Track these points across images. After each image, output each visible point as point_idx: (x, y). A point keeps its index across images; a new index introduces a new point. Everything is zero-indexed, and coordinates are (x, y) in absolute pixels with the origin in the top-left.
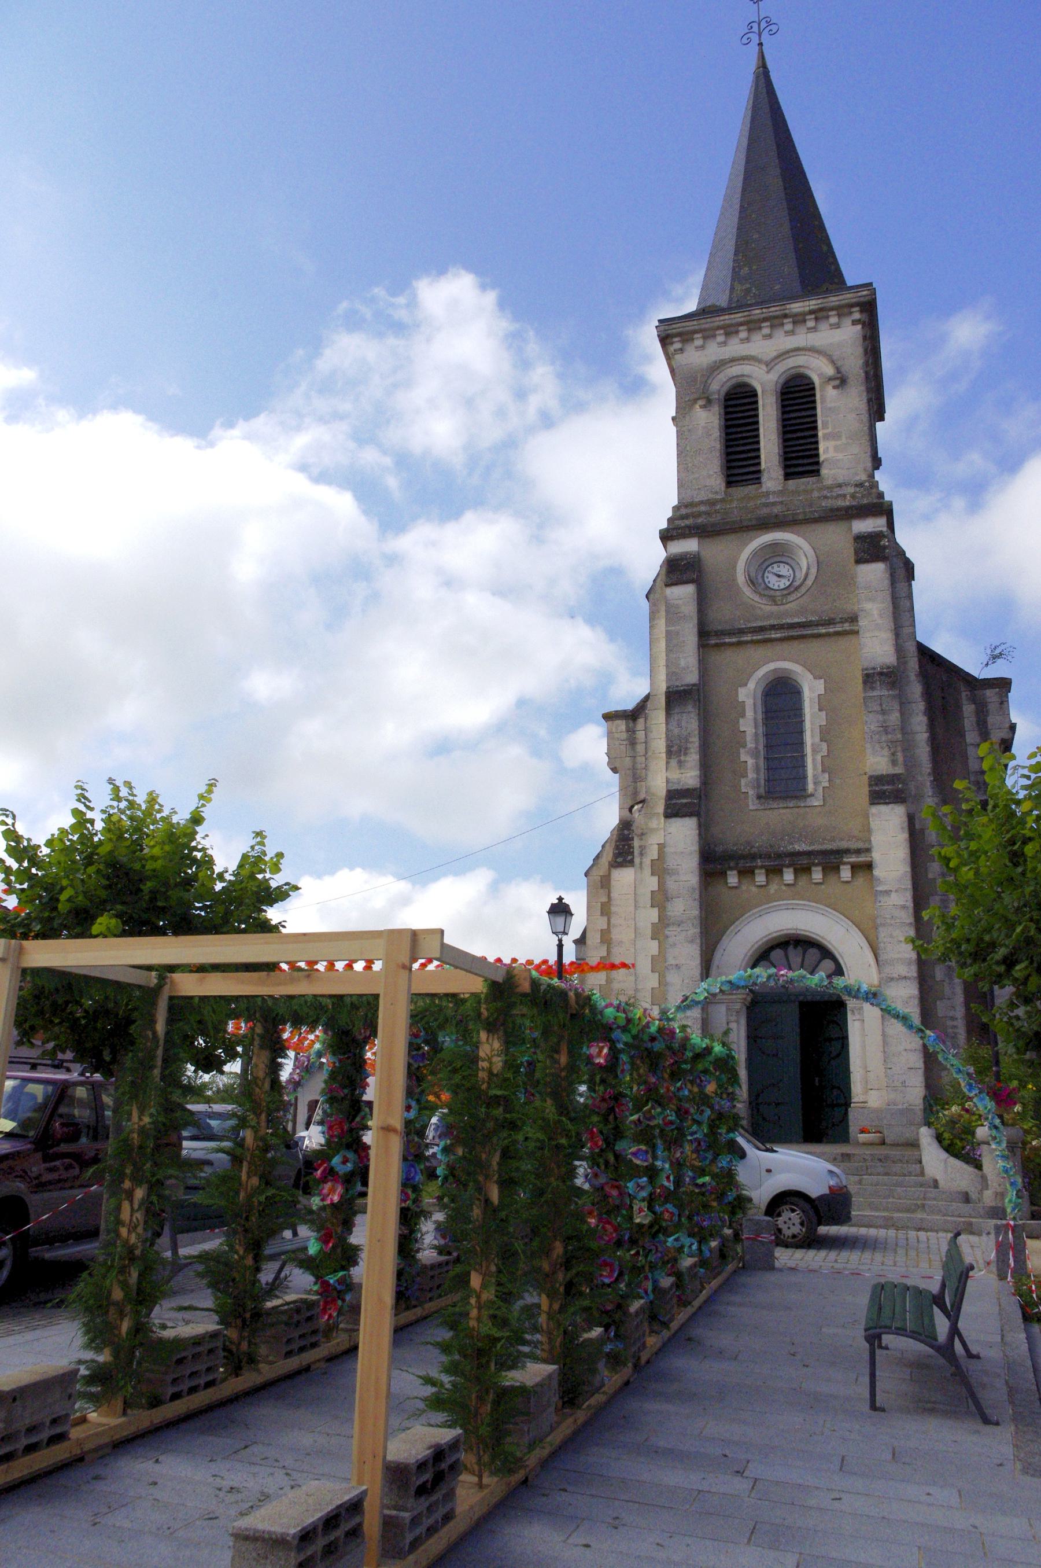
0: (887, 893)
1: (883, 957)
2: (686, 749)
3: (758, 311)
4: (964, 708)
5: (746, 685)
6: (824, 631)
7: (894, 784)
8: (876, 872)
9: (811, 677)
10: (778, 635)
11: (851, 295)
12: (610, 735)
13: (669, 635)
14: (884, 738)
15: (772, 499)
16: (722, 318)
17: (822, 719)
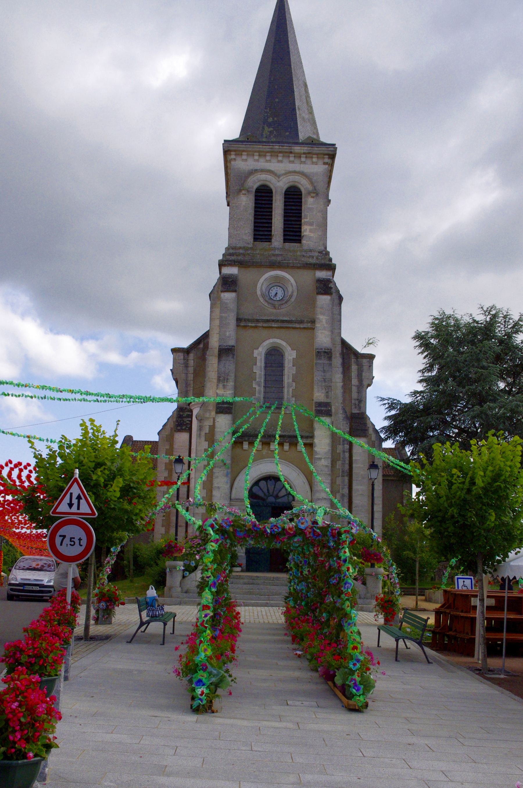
0: (320, 459)
1: (315, 488)
2: (228, 379)
3: (277, 147)
4: (353, 367)
5: (258, 349)
6: (298, 326)
7: (327, 407)
8: (316, 449)
9: (290, 349)
10: (276, 325)
11: (325, 149)
12: (174, 359)
13: (221, 318)
14: (324, 384)
15: (277, 252)
16: (259, 147)
17: (294, 371)
